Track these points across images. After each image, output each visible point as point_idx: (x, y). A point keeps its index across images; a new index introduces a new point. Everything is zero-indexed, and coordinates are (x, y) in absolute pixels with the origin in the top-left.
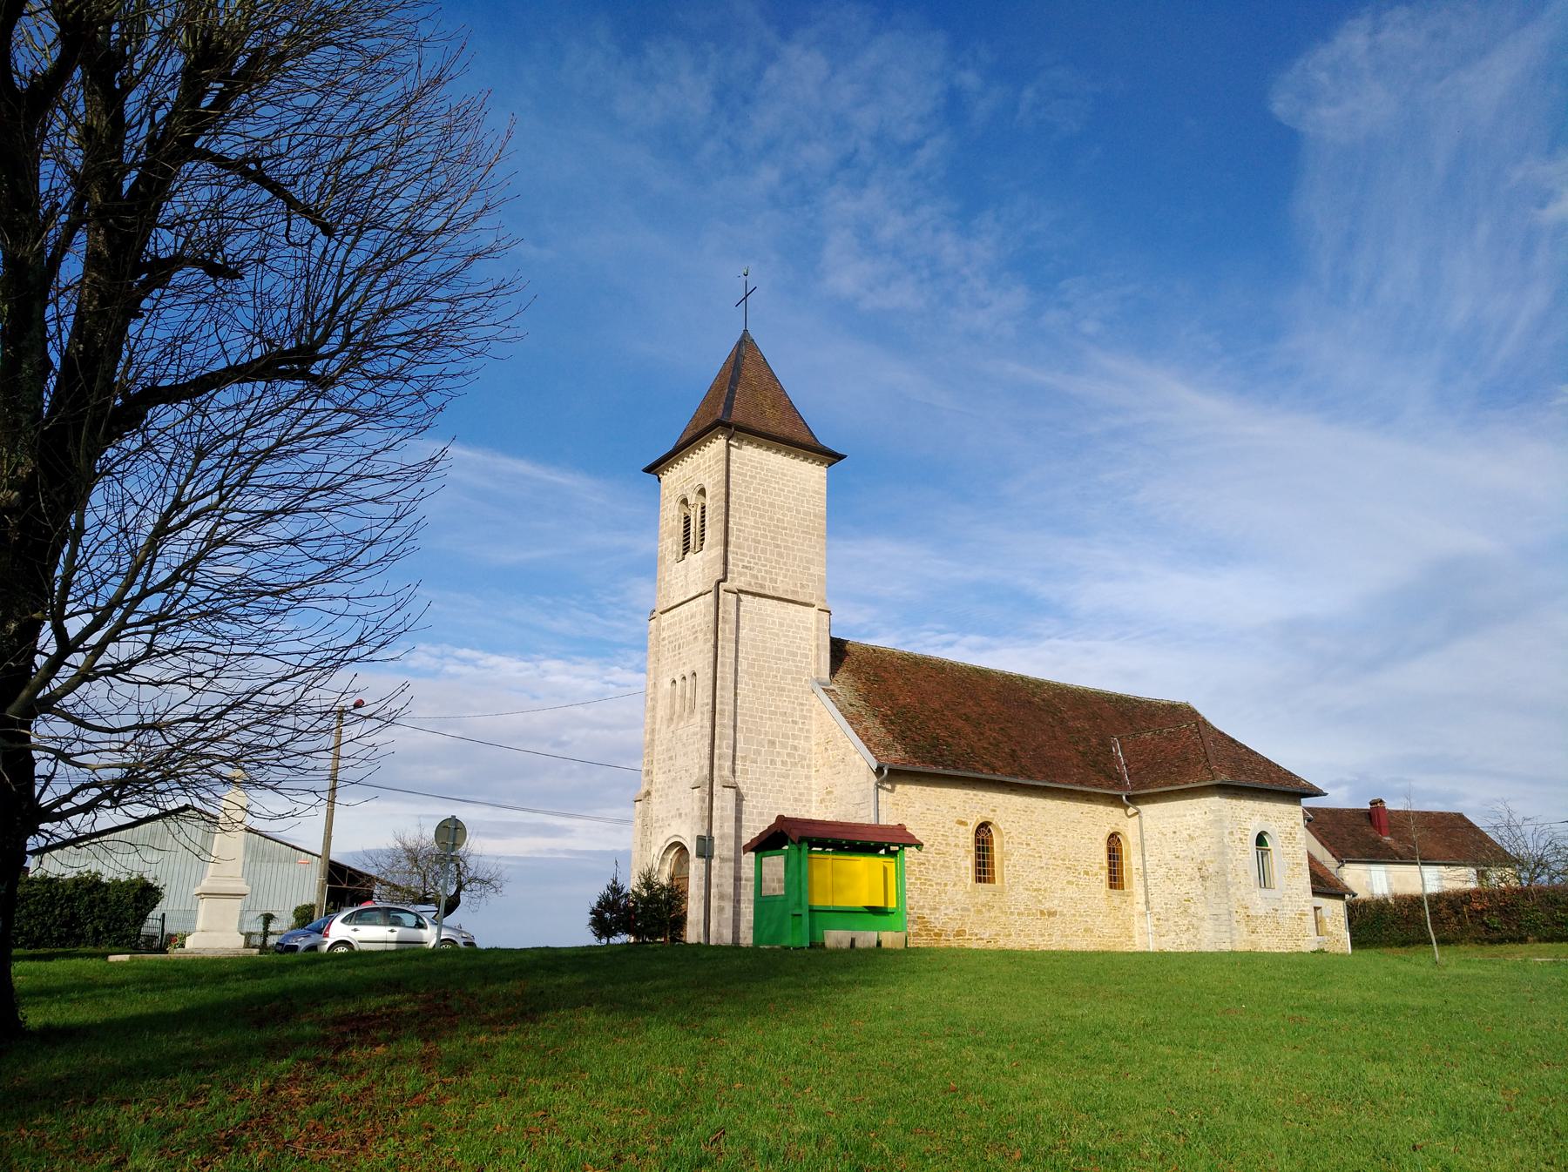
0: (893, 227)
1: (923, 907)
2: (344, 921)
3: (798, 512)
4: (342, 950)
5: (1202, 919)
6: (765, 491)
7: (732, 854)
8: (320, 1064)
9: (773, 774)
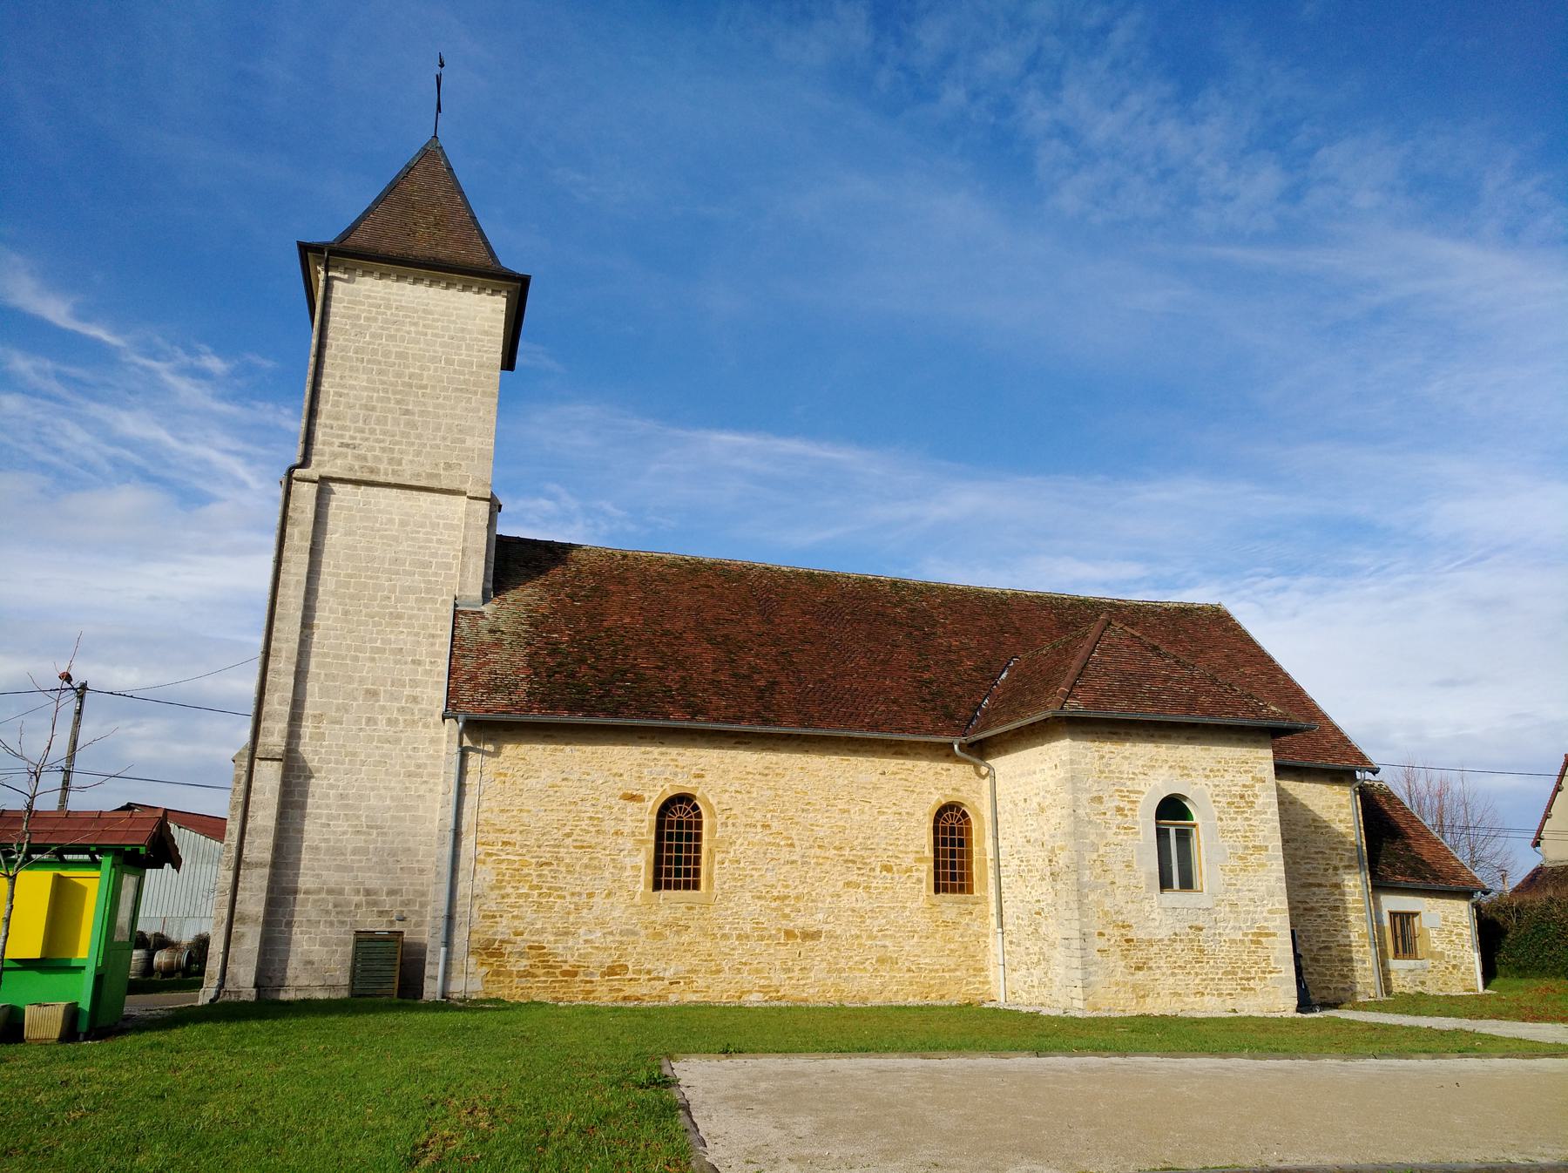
0: (1104, 127)
1: (542, 931)
3: (448, 362)
5: (1053, 945)
6: (391, 337)
7: (268, 856)
9: (370, 739)
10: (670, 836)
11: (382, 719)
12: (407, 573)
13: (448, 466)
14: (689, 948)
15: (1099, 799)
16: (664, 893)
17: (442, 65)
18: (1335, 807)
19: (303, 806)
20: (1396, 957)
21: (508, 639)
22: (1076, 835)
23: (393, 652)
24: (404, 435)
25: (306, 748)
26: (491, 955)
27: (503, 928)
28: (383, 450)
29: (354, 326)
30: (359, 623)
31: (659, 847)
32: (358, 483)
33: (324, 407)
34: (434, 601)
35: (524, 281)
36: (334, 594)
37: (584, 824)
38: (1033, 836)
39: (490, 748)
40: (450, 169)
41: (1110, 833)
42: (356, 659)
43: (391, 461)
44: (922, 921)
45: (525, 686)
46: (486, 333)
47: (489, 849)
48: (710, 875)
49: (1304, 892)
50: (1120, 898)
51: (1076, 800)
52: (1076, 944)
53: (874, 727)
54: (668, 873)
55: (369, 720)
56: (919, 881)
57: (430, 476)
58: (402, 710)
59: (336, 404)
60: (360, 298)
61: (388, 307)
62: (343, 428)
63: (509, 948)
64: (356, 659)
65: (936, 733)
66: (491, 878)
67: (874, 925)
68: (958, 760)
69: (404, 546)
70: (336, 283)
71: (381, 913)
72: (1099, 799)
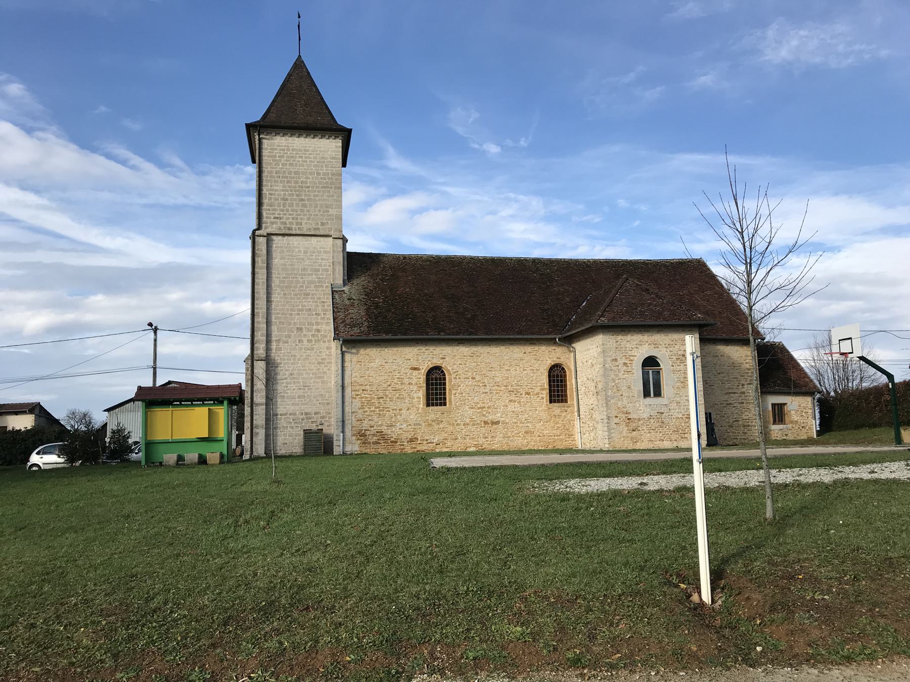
2: (38, 453)
4: (35, 468)
5: (597, 422)
6: (291, 165)
7: (264, 401)
8: (238, 500)
9: (301, 349)
10: (432, 384)
11: (305, 340)
12: (309, 275)
13: (323, 224)
14: (443, 430)
15: (616, 360)
16: (431, 408)
17: (299, 17)
18: (743, 357)
19: (276, 379)
20: (774, 423)
21: (356, 302)
22: (605, 375)
23: (307, 310)
24: (302, 211)
25: (273, 354)
26: (361, 436)
27: (366, 424)
28: (293, 218)
29: (274, 160)
30: (291, 298)
31: (428, 389)
32: (283, 235)
33: (265, 201)
34: (322, 286)
35: (350, 131)
36: (279, 286)
37: (395, 381)
38: (590, 377)
39: (354, 351)
40: (309, 73)
41: (620, 374)
42: (291, 314)
43: (297, 223)
44: (544, 415)
45: (366, 324)
46: (333, 158)
47: (357, 393)
48: (450, 401)
49: (727, 396)
50: (625, 402)
51: (605, 361)
52: (606, 421)
53: (519, 333)
54: (433, 399)
55: (299, 341)
56: (543, 398)
57: (315, 229)
58: (313, 335)
59: (270, 199)
60: (276, 146)
61: (288, 150)
62: (274, 210)
63: (368, 433)
64: (291, 314)
65: (548, 333)
66: (359, 405)
67: (523, 417)
68: (560, 345)
69: (307, 262)
70: (264, 141)
71: (312, 422)
72: (616, 360)
